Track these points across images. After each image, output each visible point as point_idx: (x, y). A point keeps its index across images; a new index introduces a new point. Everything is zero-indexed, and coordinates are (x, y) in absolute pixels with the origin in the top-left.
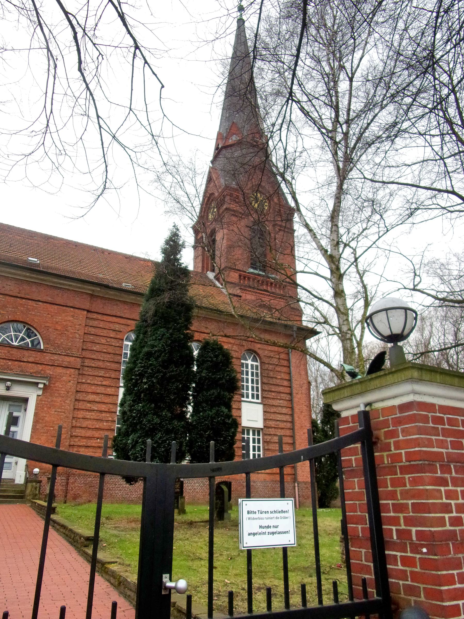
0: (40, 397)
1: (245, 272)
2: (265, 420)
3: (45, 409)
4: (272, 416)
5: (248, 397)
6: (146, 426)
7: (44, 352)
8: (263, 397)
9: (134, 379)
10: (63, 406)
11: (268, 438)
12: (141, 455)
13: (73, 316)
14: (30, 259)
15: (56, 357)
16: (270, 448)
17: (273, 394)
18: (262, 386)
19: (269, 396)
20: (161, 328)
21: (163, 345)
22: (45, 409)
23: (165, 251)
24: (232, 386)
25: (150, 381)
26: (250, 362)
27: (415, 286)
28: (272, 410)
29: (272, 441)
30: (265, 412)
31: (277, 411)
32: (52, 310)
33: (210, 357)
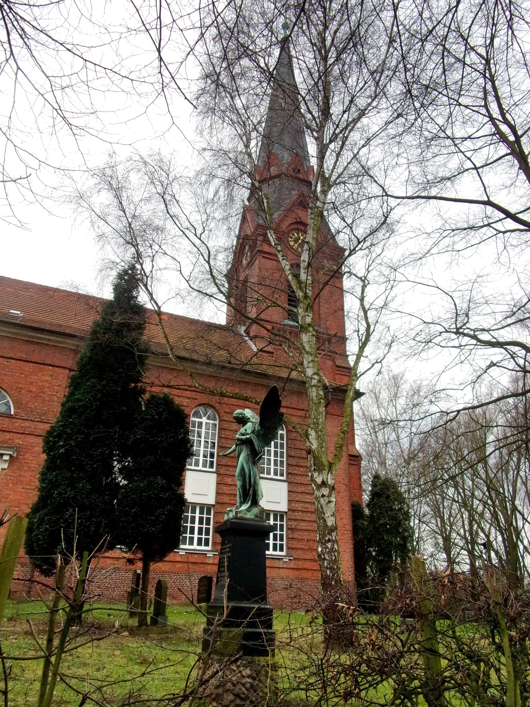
0: (5, 471)
1: (280, 324)
2: (290, 501)
3: (11, 485)
4: (300, 497)
5: (269, 473)
6: (56, 500)
7: (13, 418)
8: (288, 474)
9: (51, 441)
10: (33, 482)
11: (293, 524)
12: (44, 537)
13: (51, 376)
14: (12, 311)
15: (27, 424)
16: (295, 536)
17: (301, 469)
18: (287, 460)
19: (295, 472)
20: (94, 377)
21: (90, 399)
22: (11, 485)
23: (117, 288)
24: (182, 452)
25: (68, 444)
26: (204, 420)
27: (458, 329)
28: (300, 489)
29: (298, 527)
30: (289, 491)
31: (306, 491)
32: (27, 369)
33: (151, 415)
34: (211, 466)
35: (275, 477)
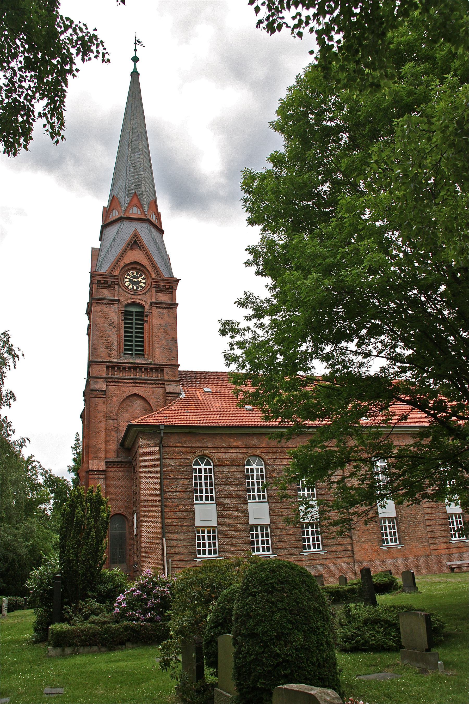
34: (212, 499)
35: (260, 501)
